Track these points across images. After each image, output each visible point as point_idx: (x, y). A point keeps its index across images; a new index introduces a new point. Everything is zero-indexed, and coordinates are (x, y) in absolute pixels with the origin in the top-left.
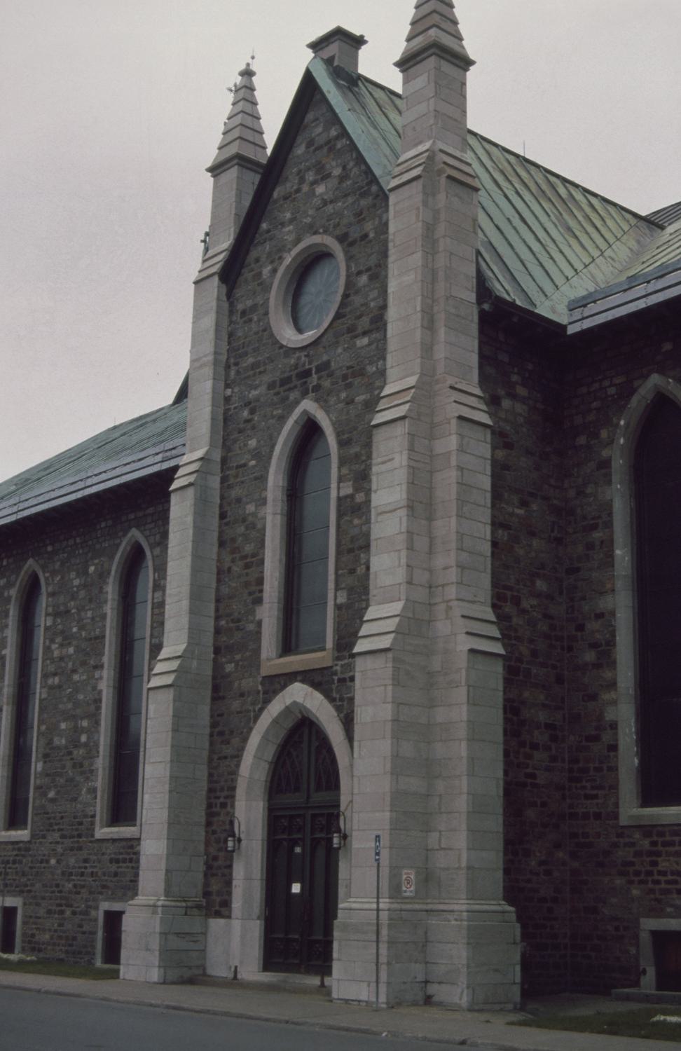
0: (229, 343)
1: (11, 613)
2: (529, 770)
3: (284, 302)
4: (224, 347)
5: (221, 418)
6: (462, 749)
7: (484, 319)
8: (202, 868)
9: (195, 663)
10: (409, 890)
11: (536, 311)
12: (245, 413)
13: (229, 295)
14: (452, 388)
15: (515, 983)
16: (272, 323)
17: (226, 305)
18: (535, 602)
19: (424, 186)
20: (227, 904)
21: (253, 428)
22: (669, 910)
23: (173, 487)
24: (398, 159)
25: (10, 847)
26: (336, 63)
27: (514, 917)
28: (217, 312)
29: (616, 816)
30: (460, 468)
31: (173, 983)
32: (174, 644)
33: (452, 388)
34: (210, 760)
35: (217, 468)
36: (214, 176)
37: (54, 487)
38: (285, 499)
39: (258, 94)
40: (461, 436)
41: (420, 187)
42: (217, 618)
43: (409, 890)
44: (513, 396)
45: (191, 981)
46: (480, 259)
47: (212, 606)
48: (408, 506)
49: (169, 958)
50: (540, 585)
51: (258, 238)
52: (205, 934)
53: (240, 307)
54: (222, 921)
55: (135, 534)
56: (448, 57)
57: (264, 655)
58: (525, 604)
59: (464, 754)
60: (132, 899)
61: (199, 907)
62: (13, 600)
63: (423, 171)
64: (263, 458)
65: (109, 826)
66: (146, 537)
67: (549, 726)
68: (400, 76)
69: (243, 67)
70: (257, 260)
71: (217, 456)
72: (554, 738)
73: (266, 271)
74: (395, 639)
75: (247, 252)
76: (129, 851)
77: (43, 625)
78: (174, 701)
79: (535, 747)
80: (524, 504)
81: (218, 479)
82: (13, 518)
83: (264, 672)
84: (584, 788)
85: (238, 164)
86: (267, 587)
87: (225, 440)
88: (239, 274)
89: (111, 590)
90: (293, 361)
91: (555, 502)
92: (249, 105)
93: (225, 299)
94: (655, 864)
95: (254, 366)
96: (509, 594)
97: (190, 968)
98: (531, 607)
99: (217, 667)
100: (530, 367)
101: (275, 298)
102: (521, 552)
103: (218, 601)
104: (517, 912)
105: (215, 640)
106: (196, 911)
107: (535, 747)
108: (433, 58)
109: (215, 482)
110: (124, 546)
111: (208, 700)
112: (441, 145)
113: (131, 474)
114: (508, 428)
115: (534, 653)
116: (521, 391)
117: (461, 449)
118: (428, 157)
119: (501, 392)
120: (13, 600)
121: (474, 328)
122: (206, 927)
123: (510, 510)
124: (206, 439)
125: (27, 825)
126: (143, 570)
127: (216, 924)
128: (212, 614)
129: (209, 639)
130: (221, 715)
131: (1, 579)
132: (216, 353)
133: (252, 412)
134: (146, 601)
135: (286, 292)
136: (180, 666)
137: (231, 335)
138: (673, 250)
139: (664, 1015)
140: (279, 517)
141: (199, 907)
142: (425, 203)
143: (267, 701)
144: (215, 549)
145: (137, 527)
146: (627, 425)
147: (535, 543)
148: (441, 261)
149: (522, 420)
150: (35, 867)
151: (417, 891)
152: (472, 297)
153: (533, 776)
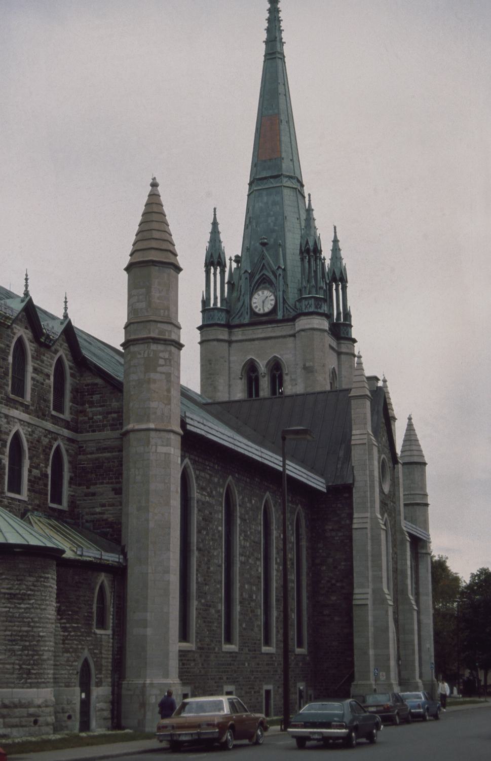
25: (228, 655)
39: (364, 366)
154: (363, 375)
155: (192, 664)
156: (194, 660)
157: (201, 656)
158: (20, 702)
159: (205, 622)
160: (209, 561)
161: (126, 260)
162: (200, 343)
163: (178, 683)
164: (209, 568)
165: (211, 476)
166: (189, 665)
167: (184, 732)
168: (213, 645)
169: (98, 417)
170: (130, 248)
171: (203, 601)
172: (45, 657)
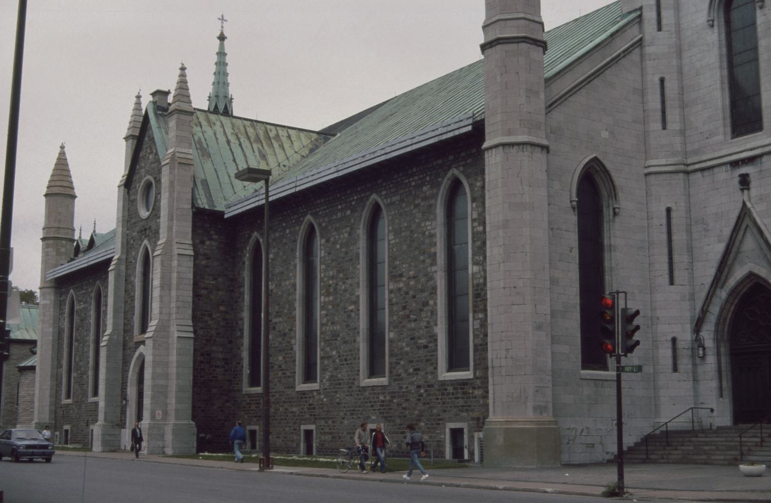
0: (128, 212)
1: (92, 304)
2: (215, 375)
3: (143, 199)
4: (127, 214)
5: (125, 242)
6: (174, 370)
7: (194, 213)
8: (120, 411)
9: (115, 337)
10: (158, 417)
11: (215, 209)
12: (132, 242)
13: (128, 193)
14: (177, 243)
15: (193, 447)
16: (138, 208)
17: (127, 197)
18: (218, 315)
19: (170, 167)
20: (125, 424)
21: (134, 247)
22: (252, 423)
23: (110, 269)
24: (167, 151)
25: (93, 404)
26: (158, 104)
27: (194, 425)
28: (123, 201)
29: (242, 391)
30: (177, 272)
31: (107, 452)
32: (109, 331)
33: (177, 243)
34: (122, 372)
35: (124, 262)
36: (126, 141)
37: (348, 160)
38: (142, 276)
39: (188, 78)
40: (179, 260)
41: (168, 168)
42: (124, 319)
43: (158, 417)
44: (211, 239)
45: (114, 451)
46: (196, 189)
47: (122, 315)
48: (160, 286)
49: (105, 443)
50: (222, 308)
51: (136, 172)
52: (120, 434)
53: (131, 199)
54: (124, 430)
55: (374, 196)
56: (184, 113)
57: (135, 334)
58: (214, 316)
59: (175, 372)
60: (96, 423)
61: (118, 425)
62: (93, 298)
63: (170, 161)
64: (135, 259)
65: (369, 378)
66: (382, 200)
67: (223, 359)
68: (125, 142)
69: (137, 94)
70: (136, 181)
71: (124, 257)
72: (227, 364)
73: (138, 185)
74: (154, 334)
75: (133, 177)
76: (96, 404)
77: (319, 256)
78: (107, 351)
79: (218, 367)
80: (215, 279)
81: (125, 266)
82: (86, 265)
83: (135, 340)
84: (236, 381)
85: (132, 138)
86: (136, 308)
87: (127, 251)
88: (131, 186)
89: (361, 233)
90: (143, 224)
91: (231, 276)
92: (138, 111)
93: (127, 194)
94: (250, 407)
95: (135, 223)
96: (207, 313)
97: (114, 447)
98: (218, 317)
99: (124, 338)
100: (220, 227)
101: (139, 197)
102: (212, 297)
103: (125, 313)
104: (196, 424)
105: (124, 327)
106: (117, 427)
107: (218, 367)
108: (176, 115)
109: (123, 267)
110: (369, 204)
111: (122, 350)
112: (178, 149)
113: (351, 168)
114: (208, 252)
115: (218, 334)
116: (215, 237)
117: (179, 265)
118: (173, 155)
119: (205, 239)
120: (93, 298)
121: (190, 218)
122: (121, 432)
123: (208, 282)
124: (119, 250)
125: (468, 366)
126: (380, 220)
127: (123, 430)
128: (123, 318)
129: (122, 327)
130: (125, 356)
131: (1, 320)
132: (123, 217)
133: (134, 241)
134: (384, 239)
135: (143, 195)
136: (109, 338)
137: (129, 209)
138: (477, 106)
139: (333, 462)
140: (140, 283)
141: (118, 425)
142: (170, 173)
143: (135, 351)
144: (124, 293)
145: (376, 193)
146: (249, 249)
147: (220, 293)
148: (176, 195)
149: (214, 248)
150: (342, 403)
151: (162, 418)
152: (190, 206)
153: (216, 377)
154: (191, 106)
155: (71, 412)
156: (72, 409)
157: (76, 406)
158: (542, 150)
159: (79, 385)
160: (84, 345)
161: (44, 191)
162: (46, 195)
163: (495, 151)
164: (83, 350)
165: (86, 289)
166: (70, 412)
167: (589, 45)
168: (84, 399)
169: (203, 291)
170: (47, 184)
171: (79, 372)
172: (19, 412)
